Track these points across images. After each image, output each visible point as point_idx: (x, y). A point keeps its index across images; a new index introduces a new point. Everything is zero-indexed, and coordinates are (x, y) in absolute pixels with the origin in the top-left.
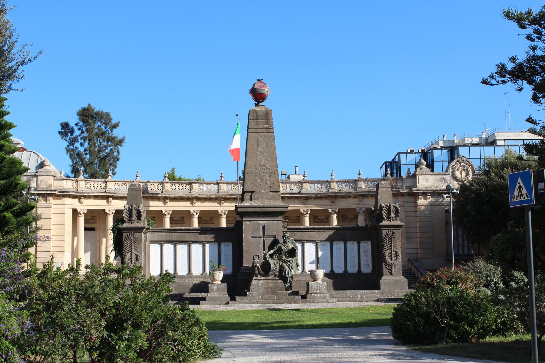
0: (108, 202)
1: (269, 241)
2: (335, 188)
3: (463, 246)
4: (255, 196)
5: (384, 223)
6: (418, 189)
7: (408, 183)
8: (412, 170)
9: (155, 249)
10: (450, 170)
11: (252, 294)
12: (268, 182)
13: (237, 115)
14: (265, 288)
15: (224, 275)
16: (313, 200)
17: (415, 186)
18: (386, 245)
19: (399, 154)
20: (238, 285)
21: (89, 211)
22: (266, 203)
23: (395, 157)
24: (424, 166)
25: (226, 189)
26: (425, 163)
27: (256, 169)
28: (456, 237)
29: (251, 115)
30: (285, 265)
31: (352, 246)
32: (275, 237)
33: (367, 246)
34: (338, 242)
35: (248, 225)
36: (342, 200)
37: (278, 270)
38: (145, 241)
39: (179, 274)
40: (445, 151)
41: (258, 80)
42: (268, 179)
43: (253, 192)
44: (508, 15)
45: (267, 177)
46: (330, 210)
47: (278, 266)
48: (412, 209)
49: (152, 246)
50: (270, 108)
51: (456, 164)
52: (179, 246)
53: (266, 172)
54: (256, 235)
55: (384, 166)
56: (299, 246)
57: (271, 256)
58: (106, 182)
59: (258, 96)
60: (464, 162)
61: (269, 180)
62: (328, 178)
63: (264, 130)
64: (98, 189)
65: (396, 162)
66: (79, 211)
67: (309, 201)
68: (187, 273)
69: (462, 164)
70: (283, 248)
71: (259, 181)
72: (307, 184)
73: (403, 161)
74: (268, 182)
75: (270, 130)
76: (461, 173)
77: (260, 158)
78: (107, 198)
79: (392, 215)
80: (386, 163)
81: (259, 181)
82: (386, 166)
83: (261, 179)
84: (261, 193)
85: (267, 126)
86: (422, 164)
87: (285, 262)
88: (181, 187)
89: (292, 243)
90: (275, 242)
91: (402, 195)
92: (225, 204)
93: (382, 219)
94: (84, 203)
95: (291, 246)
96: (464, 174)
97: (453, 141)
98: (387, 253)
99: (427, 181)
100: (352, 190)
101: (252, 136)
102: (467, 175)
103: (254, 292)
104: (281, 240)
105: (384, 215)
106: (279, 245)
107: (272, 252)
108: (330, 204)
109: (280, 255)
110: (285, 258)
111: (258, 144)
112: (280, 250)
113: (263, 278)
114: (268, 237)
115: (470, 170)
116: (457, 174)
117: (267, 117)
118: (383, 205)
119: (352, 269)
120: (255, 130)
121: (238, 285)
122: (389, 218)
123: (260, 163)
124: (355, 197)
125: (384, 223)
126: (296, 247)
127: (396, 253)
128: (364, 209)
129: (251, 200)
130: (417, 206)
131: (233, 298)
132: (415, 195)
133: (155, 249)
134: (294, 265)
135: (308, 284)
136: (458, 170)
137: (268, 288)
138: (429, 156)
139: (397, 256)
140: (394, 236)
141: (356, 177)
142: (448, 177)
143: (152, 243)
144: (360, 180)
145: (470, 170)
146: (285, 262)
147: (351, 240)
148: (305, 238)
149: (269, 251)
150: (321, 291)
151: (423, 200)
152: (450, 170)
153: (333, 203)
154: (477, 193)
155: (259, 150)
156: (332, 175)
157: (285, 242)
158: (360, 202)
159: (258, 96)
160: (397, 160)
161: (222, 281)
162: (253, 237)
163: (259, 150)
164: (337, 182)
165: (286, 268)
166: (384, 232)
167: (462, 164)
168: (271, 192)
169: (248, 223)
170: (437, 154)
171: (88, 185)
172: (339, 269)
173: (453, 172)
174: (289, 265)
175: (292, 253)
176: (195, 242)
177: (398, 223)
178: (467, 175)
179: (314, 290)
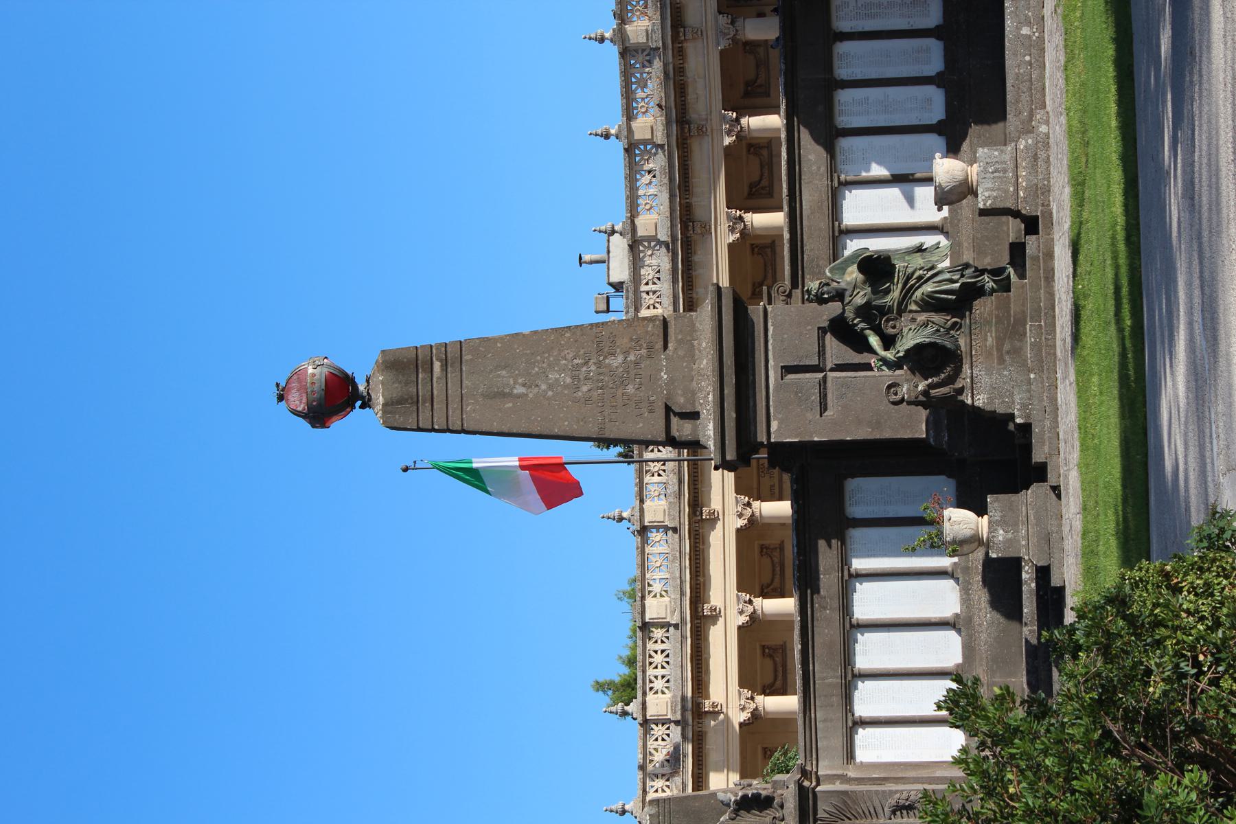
1: (836, 351)
2: (649, 123)
4: (680, 403)
9: (873, 748)
11: (1024, 407)
12: (631, 358)
13: (406, 470)
14: (1001, 360)
15: (961, 504)
16: (694, 200)
20: (994, 458)
22: (706, 363)
25: (663, 503)
27: (587, 400)
29: (399, 420)
30: (918, 294)
32: (822, 331)
34: (837, 109)
35: (781, 427)
36: (691, 97)
37: (937, 318)
38: (844, 779)
39: (959, 660)
41: (281, 398)
42: (620, 358)
43: (668, 409)
45: (616, 362)
46: (727, 141)
47: (922, 317)
49: (862, 755)
50: (376, 356)
53: (599, 364)
54: (816, 398)
56: (853, 246)
57: (888, 342)
59: (335, 398)
61: (626, 353)
63: (453, 375)
67: (698, 213)
70: (859, 300)
71: (630, 389)
72: (639, 221)
74: (631, 358)
75: (453, 356)
77: (550, 387)
81: (630, 389)
83: (623, 382)
84: (671, 381)
85: (437, 366)
87: (907, 292)
88: (659, 658)
89: (842, 269)
90: (841, 329)
92: (715, 504)
95: (853, 274)
103: (1017, 398)
104: (834, 308)
107: (874, 340)
109: (883, 311)
110: (896, 294)
111: (503, 395)
112: (865, 311)
113: (966, 369)
114: (822, 352)
117: (406, 365)
119: (932, 57)
120: (455, 405)
121: (994, 458)
123: (566, 386)
124: (680, 53)
126: (856, 254)
128: (723, 20)
129: (695, 416)
131: (1039, 473)
133: (873, 748)
134: (918, 261)
135: (984, 212)
137: (999, 350)
143: (850, 755)
144: (620, 36)
146: (907, 292)
147: (827, 63)
148: (824, 224)
149: (871, 350)
150: (1011, 165)
153: (702, 131)
155: (523, 390)
156: (607, 136)
157: (839, 296)
158: (699, 34)
159: (335, 398)
161: (981, 511)
162: (823, 407)
163: (523, 390)
164: (629, 115)
165: (929, 288)
168: (666, 347)
169: (774, 425)
174: (920, 278)
175: (877, 269)
176: (846, 607)
179: (1007, 191)
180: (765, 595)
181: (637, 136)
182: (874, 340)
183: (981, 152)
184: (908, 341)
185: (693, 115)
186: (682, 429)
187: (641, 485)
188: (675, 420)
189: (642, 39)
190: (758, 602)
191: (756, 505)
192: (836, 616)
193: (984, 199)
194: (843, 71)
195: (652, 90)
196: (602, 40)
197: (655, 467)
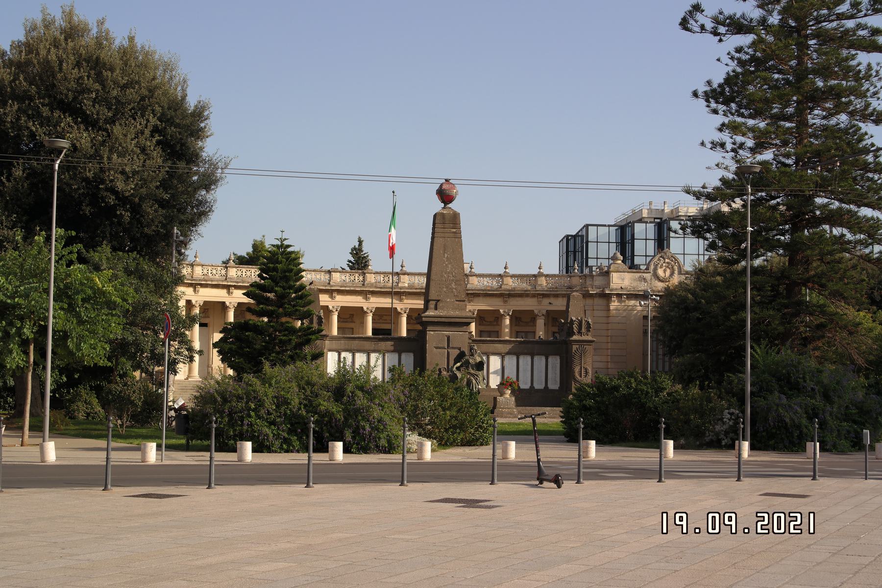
0: (229, 293)
1: (454, 353)
2: (510, 283)
3: (664, 362)
4: (440, 305)
5: (575, 337)
6: (611, 290)
7: (599, 281)
8: (605, 263)
10: (652, 267)
16: (481, 298)
17: (608, 284)
18: (576, 361)
19: (587, 226)
21: (206, 303)
22: (452, 313)
23: (581, 230)
24: (620, 262)
25: (373, 281)
26: (622, 258)
27: (442, 276)
28: (655, 349)
29: (438, 217)
31: (540, 361)
32: (460, 349)
33: (555, 362)
35: (433, 336)
36: (518, 299)
40: (651, 227)
41: (446, 180)
43: (438, 301)
44: (688, 192)
45: (453, 285)
46: (501, 311)
48: (603, 314)
49: (330, 354)
50: (458, 211)
51: (659, 260)
52: (357, 355)
55: (565, 240)
56: (485, 358)
57: (458, 369)
58: (227, 267)
59: (445, 196)
60: (669, 258)
62: (501, 271)
64: (217, 276)
65: (582, 236)
66: (194, 302)
67: (476, 299)
68: (529, 385)
69: (667, 260)
70: (471, 361)
72: (474, 278)
73: (592, 236)
75: (458, 235)
76: (665, 271)
78: (228, 287)
79: (583, 330)
80: (567, 237)
82: (568, 240)
83: (447, 287)
86: (617, 259)
87: (473, 375)
89: (479, 356)
90: (461, 355)
91: (592, 296)
92: (373, 299)
93: (573, 334)
94: (200, 294)
95: (478, 359)
96: (668, 272)
97: (663, 210)
98: (577, 370)
99: (623, 280)
100: (529, 288)
101: (438, 241)
102: (672, 274)
105: (575, 330)
106: (467, 357)
107: (458, 364)
108: (502, 304)
109: (467, 367)
110: (472, 372)
111: (445, 250)
112: (467, 362)
114: (453, 348)
115: (676, 268)
116: (660, 272)
117: (455, 219)
118: (574, 319)
119: (539, 385)
120: (442, 235)
122: (580, 333)
124: (534, 296)
125: (575, 337)
127: (586, 369)
128: (544, 312)
129: (436, 309)
130: (609, 310)
132: (607, 297)
134: (481, 379)
135: (495, 399)
136: (661, 267)
138: (628, 230)
139: (586, 373)
140: (584, 351)
141: (535, 272)
142: (648, 276)
143: (330, 350)
144: (540, 275)
145: (676, 268)
146: (473, 375)
147: (539, 354)
148: (491, 350)
149: (455, 363)
151: (616, 304)
152: (652, 267)
153: (505, 302)
154: (684, 300)
156: (505, 268)
157: (472, 355)
159: (445, 196)
160: (584, 233)
162: (437, 348)
164: (513, 276)
165: (474, 381)
166: (574, 347)
167: (667, 260)
170: (639, 228)
171: (205, 271)
172: (525, 385)
173: (655, 270)
175: (480, 366)
176: (374, 351)
177: (589, 338)
178: (672, 274)
180: (338, 316)
181: (505, 279)
182: (458, 364)
183: (513, 398)
184: (459, 375)
185: (511, 299)
186: (432, 305)
187: (380, 273)
188: (434, 302)
189: (539, 283)
190: (336, 313)
191: (371, 314)
192: (372, 348)
193: (499, 399)
194: (536, 358)
195: (525, 286)
196: (540, 268)
197: (386, 279)
